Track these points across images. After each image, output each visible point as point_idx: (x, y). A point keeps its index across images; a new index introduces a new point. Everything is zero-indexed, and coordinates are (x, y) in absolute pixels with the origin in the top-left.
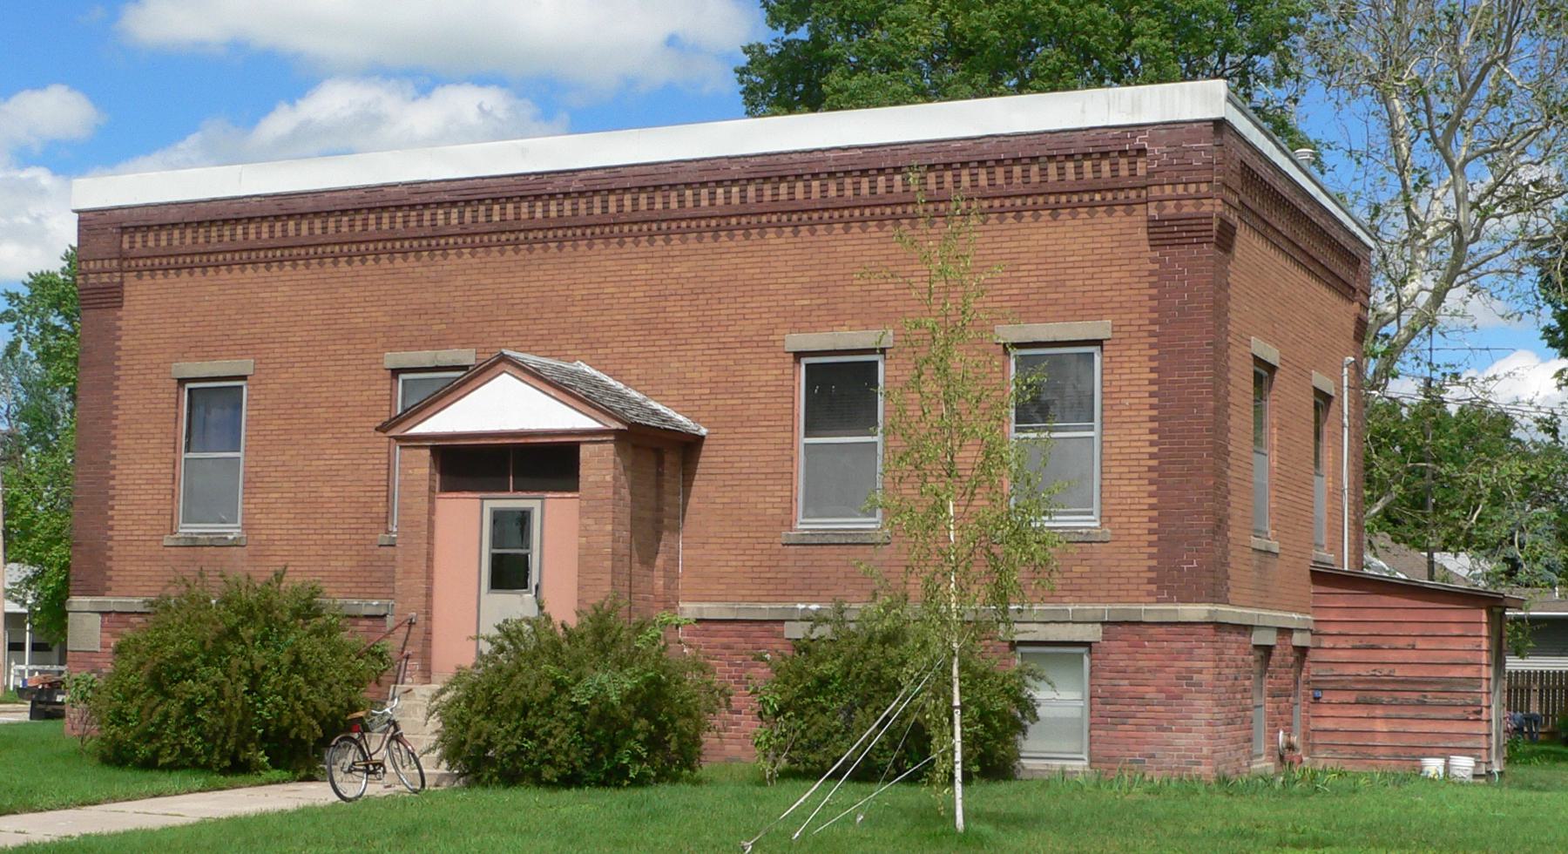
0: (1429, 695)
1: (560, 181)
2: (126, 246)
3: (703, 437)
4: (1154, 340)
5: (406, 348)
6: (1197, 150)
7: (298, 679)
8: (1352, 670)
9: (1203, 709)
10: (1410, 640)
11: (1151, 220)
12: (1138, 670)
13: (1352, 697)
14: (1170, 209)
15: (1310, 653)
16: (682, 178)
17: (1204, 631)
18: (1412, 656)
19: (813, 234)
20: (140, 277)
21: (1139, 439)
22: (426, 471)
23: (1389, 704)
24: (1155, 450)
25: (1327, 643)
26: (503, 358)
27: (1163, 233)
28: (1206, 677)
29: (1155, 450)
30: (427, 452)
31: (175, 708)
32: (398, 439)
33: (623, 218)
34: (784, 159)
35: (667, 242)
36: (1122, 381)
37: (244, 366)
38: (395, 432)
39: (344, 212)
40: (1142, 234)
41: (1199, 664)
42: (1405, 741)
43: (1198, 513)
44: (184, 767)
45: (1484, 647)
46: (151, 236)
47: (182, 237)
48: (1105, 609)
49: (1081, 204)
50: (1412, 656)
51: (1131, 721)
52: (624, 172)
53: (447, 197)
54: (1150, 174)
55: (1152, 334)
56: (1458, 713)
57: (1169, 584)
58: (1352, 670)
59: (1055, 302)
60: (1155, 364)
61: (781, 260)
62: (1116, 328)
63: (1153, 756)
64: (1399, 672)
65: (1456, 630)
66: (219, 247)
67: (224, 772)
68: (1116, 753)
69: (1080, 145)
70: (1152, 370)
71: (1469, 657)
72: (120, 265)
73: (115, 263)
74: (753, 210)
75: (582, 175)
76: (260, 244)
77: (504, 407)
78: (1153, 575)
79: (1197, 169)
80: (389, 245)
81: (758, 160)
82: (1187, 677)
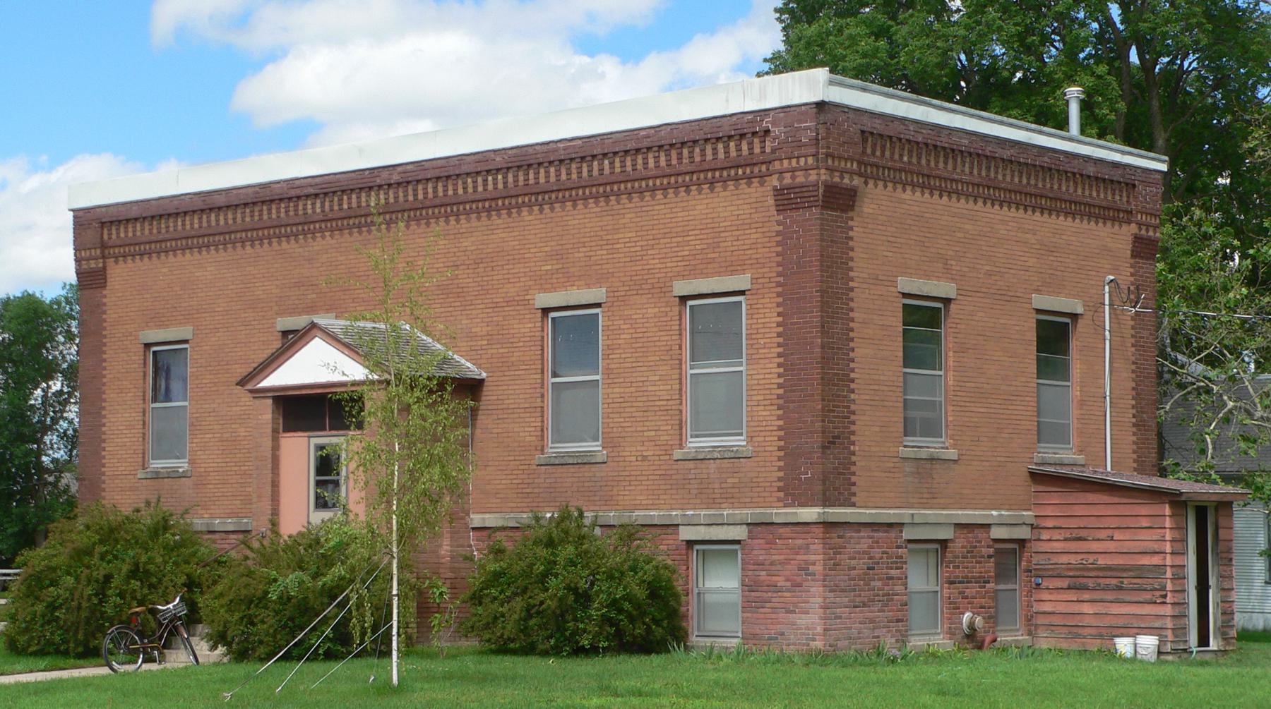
0: (1125, 581)
1: (385, 175)
2: (106, 237)
3: (482, 381)
4: (780, 289)
5: (291, 314)
6: (806, 129)
7: (135, 584)
8: (1064, 559)
9: (816, 593)
10: (1109, 532)
11: (775, 189)
12: (772, 563)
13: (1064, 583)
14: (787, 179)
15: (1028, 545)
16: (465, 169)
17: (816, 530)
18: (1110, 546)
19: (712, 192)
20: (117, 262)
21: (770, 372)
22: (270, 416)
23: (1094, 589)
24: (781, 380)
25: (1045, 536)
26: (313, 326)
27: (787, 199)
28: (818, 568)
29: (781, 380)
30: (270, 402)
31: (39, 608)
32: (251, 391)
33: (428, 203)
34: (531, 150)
35: (458, 221)
36: (760, 321)
37: (185, 332)
38: (249, 387)
39: (246, 205)
40: (771, 201)
41: (813, 558)
42: (1107, 621)
43: (811, 432)
44: (48, 654)
45: (1168, 537)
46: (674, 153)
47: (142, 229)
48: (748, 513)
49: (729, 178)
50: (1110, 546)
51: (768, 605)
52: (427, 165)
53: (312, 191)
54: (774, 151)
55: (779, 284)
56: (1148, 596)
57: (793, 493)
58: (1064, 559)
59: (713, 261)
60: (780, 309)
61: (529, 232)
62: (754, 280)
63: (783, 634)
64: (1102, 561)
65: (1145, 523)
66: (167, 236)
67: (80, 656)
68: (758, 631)
69: (726, 130)
70: (779, 314)
71: (1156, 546)
72: (102, 252)
73: (98, 251)
74: (513, 193)
75: (399, 169)
76: (193, 233)
77: (316, 365)
78: (781, 484)
79: (805, 145)
80: (733, 172)
81: (514, 151)
82: (804, 568)
